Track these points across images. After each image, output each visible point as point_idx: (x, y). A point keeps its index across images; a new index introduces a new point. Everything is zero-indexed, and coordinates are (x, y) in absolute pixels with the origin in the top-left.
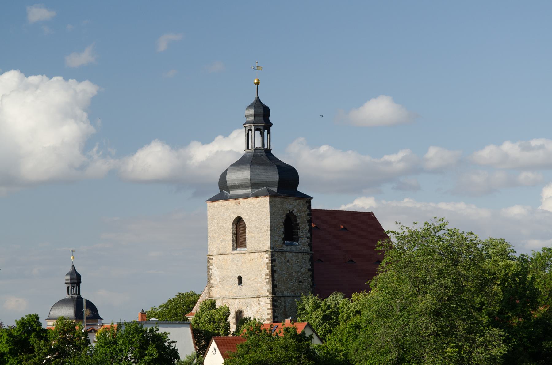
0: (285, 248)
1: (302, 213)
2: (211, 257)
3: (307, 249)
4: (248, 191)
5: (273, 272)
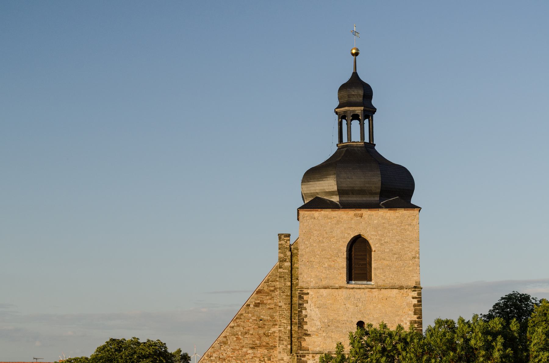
2: (305, 291)
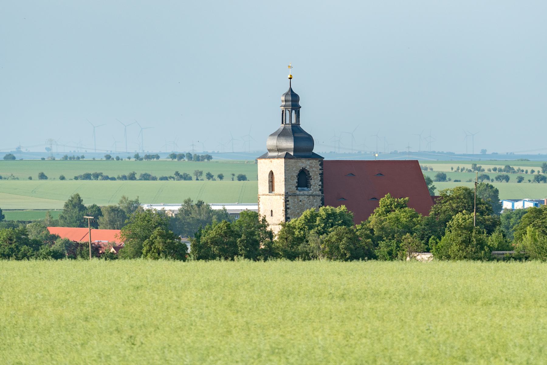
0: (298, 192)
1: (314, 169)
3: (320, 193)
4: (275, 154)
5: (286, 209)
